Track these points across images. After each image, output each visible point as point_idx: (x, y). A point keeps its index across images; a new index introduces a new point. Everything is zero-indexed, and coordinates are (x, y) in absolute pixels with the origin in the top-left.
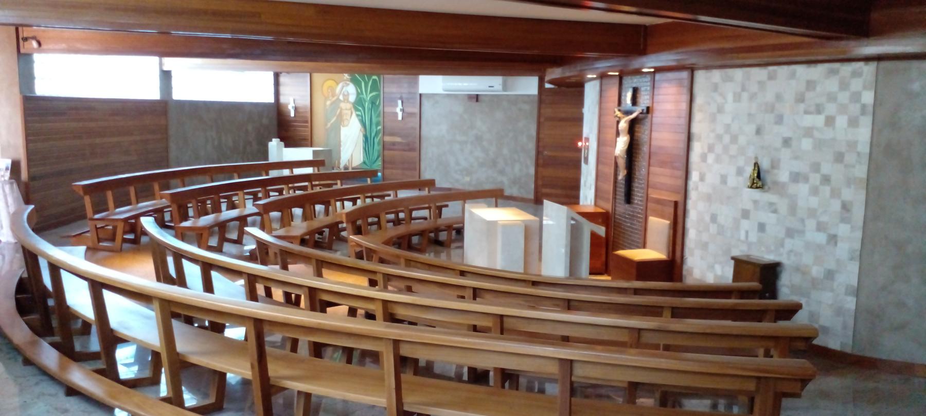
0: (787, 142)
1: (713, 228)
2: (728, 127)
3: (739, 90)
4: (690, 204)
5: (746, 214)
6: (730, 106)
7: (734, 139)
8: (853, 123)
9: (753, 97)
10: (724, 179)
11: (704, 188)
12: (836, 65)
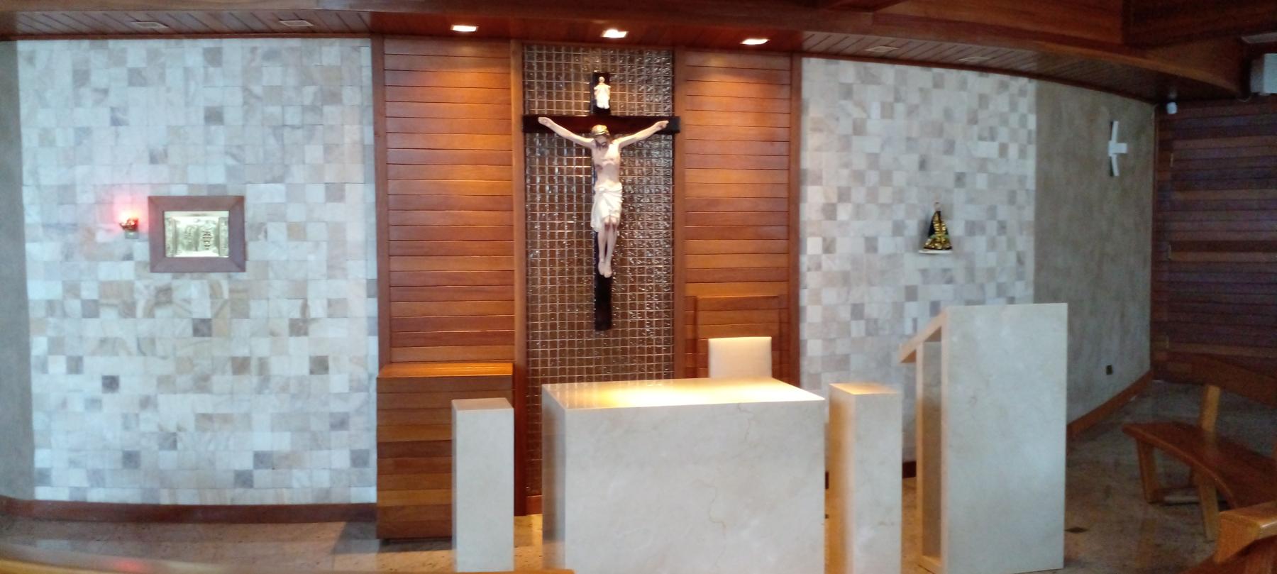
0: (960, 179)
1: (858, 329)
2: (873, 160)
3: (890, 99)
4: (805, 297)
5: (911, 293)
6: (875, 123)
7: (886, 177)
8: (1023, 153)
9: (912, 111)
10: (871, 245)
11: (833, 264)
12: (1005, 78)
